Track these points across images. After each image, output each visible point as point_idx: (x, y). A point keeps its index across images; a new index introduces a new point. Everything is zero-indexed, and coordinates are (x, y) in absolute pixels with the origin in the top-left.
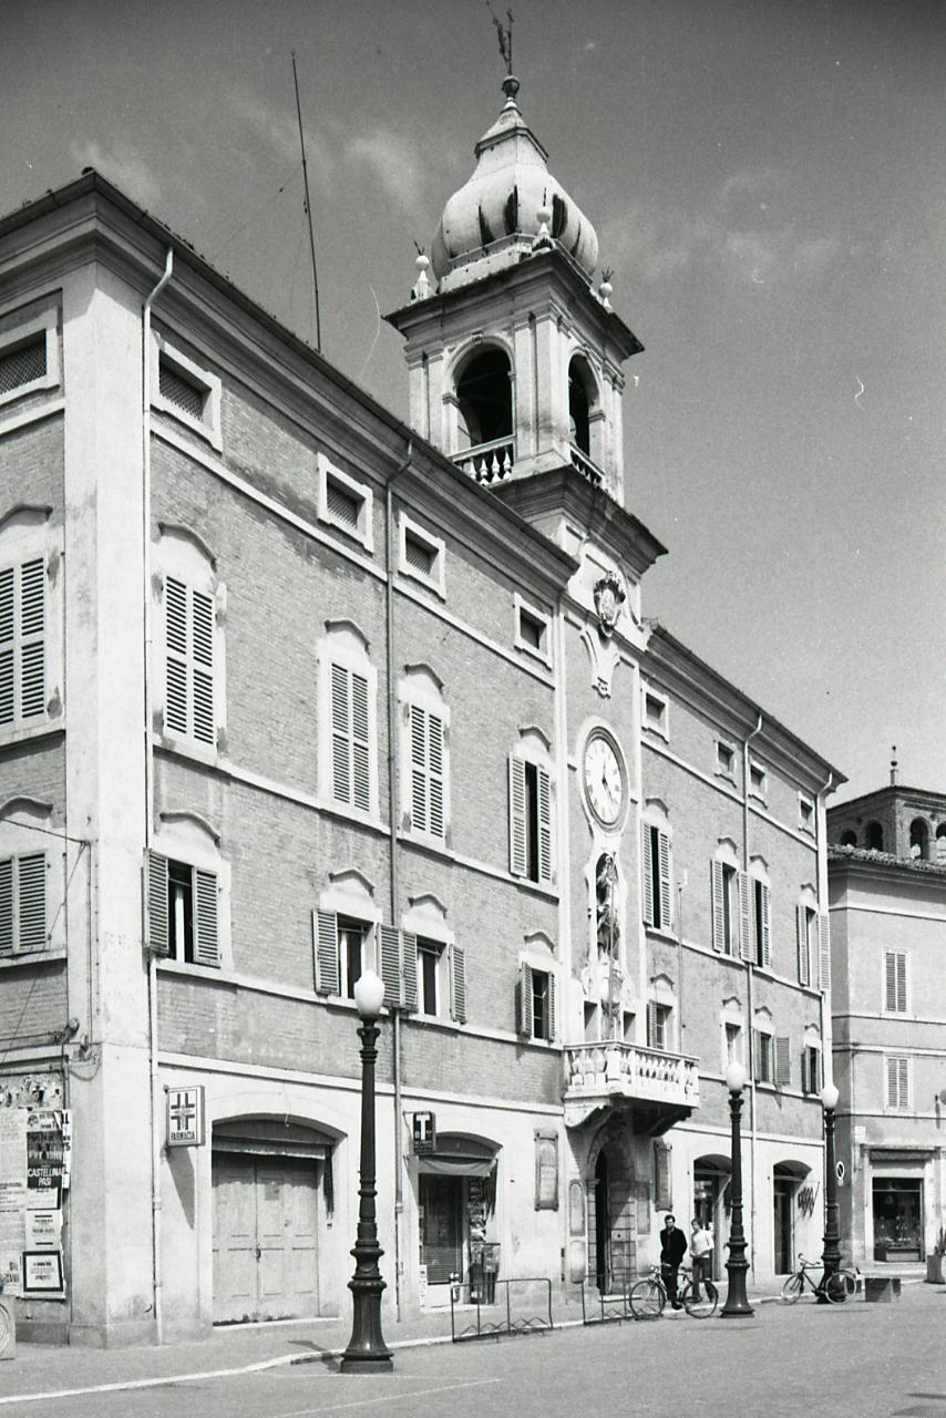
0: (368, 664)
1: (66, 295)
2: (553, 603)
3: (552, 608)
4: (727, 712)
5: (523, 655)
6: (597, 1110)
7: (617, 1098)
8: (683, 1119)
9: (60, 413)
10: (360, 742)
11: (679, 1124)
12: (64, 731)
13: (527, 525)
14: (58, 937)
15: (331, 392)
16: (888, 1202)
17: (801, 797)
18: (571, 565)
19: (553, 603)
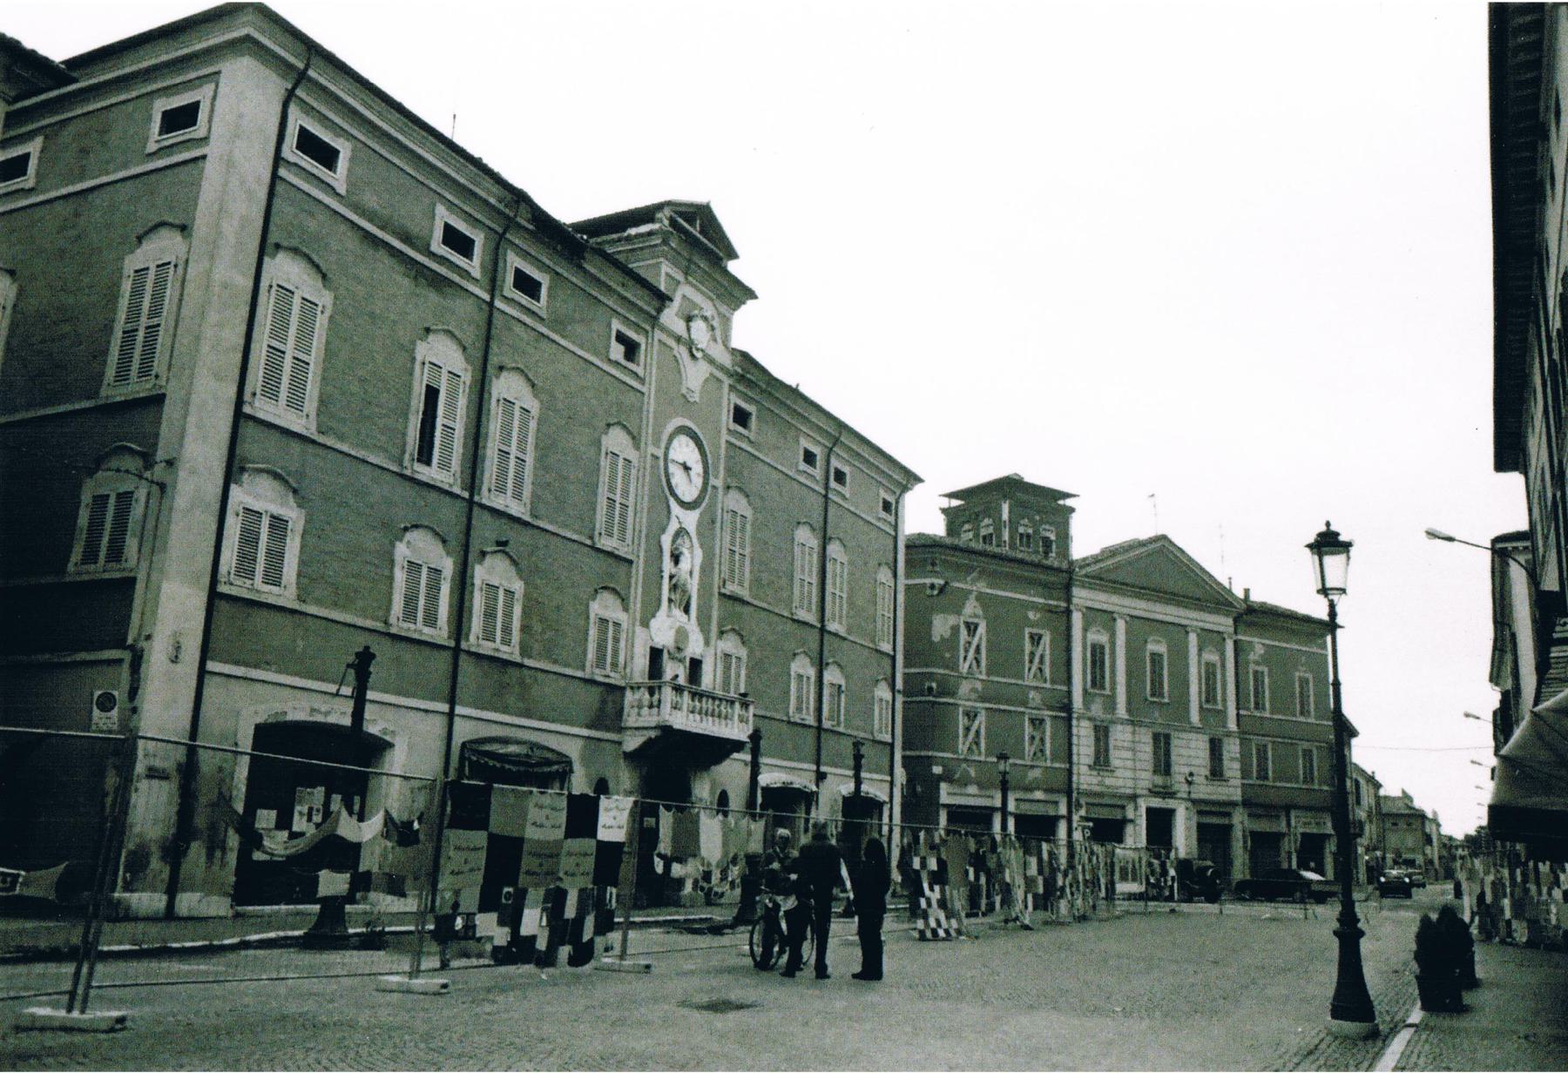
0: (531, 396)
1: (223, 80)
2: (648, 328)
3: (647, 332)
4: (820, 428)
5: (293, 169)
6: (650, 739)
7: (667, 730)
8: (738, 752)
9: (204, 157)
10: (275, 344)
11: (735, 755)
12: (164, 395)
13: (631, 270)
14: (132, 563)
15: (599, 264)
16: (324, 875)
17: (883, 494)
18: (663, 299)
19: (648, 328)
